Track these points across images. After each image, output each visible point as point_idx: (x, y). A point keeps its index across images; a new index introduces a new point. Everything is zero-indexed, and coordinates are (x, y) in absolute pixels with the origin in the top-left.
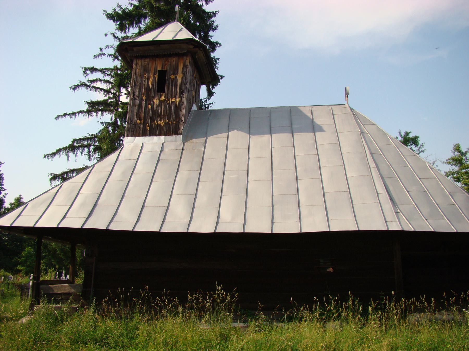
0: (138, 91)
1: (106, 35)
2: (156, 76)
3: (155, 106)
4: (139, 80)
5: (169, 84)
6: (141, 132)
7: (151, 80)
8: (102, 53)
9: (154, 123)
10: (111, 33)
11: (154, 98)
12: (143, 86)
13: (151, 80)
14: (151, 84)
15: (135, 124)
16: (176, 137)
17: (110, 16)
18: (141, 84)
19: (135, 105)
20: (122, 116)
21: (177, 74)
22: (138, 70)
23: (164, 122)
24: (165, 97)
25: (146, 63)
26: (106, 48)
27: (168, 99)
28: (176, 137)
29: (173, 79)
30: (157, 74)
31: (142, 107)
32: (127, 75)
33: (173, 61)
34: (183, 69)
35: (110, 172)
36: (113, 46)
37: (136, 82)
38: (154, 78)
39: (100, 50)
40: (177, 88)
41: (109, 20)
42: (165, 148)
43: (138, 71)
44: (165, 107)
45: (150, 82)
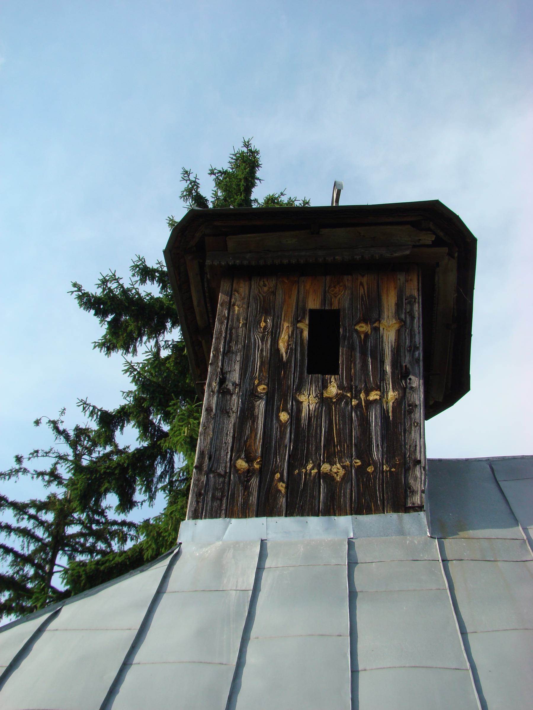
0: (237, 367)
1: (37, 423)
2: (304, 327)
3: (303, 414)
4: (241, 338)
5: (352, 348)
6: (253, 499)
7: (284, 337)
8: (21, 469)
9: (304, 470)
10: (50, 421)
11: (299, 389)
12: (257, 354)
13: (286, 337)
14: (287, 349)
15: (226, 472)
16: (400, 519)
17: (89, 300)
18: (247, 351)
19: (228, 413)
20: (83, 582)
21: (379, 320)
22: (236, 308)
23: (344, 467)
24: (340, 387)
25: (265, 289)
26: (31, 456)
27: (352, 395)
28: (400, 519)
29: (366, 335)
30: (307, 322)
31: (254, 419)
32: (108, 471)
33: (362, 284)
34: (399, 306)
35: (136, 632)
36: (49, 452)
37: (230, 341)
38: (296, 333)
39: (16, 461)
40: (382, 362)
41: (84, 309)
42: (360, 556)
43: (236, 312)
44: (346, 419)
45: (280, 341)
